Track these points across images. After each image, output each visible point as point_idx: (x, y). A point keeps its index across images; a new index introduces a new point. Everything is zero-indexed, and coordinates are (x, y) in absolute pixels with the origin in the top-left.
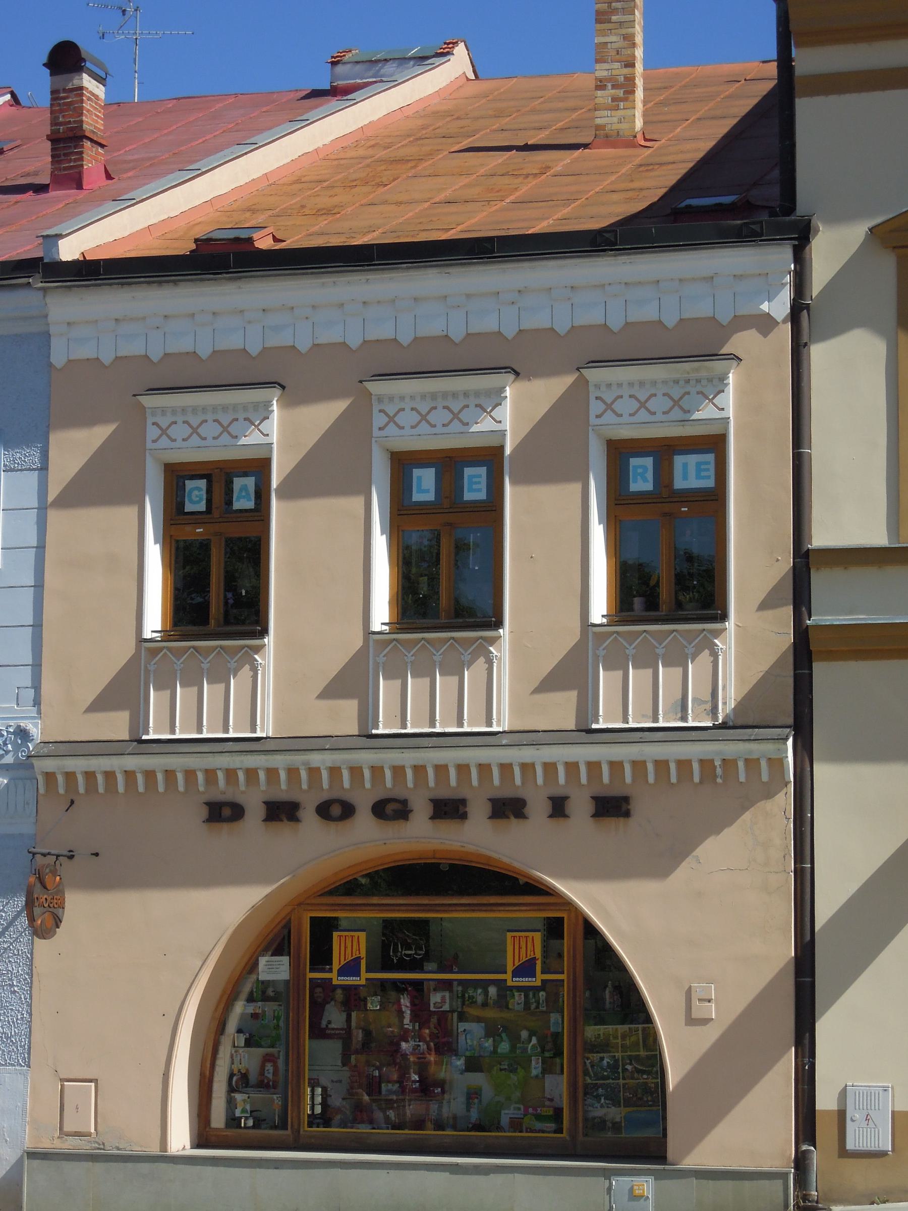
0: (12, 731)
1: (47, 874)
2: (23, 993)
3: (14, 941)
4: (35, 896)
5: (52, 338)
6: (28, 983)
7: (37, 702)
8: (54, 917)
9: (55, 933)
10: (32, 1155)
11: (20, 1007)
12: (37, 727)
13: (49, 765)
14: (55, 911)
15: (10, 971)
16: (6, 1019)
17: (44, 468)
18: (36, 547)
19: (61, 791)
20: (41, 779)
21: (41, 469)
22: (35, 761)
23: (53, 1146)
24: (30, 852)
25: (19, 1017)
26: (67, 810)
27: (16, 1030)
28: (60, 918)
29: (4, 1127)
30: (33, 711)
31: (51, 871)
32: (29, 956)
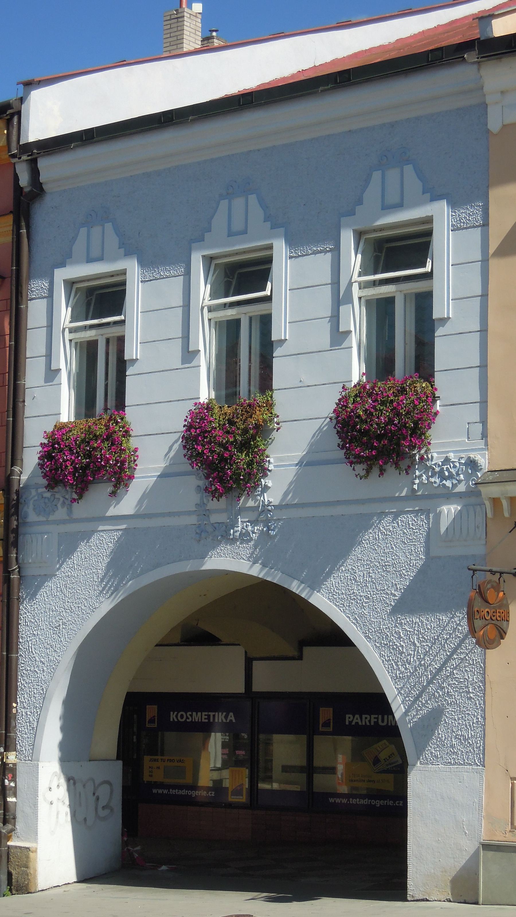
0: (464, 462)
1: (488, 589)
2: (478, 699)
3: (469, 652)
4: (476, 609)
5: (488, 107)
6: (482, 690)
7: (484, 435)
8: (496, 627)
9: (499, 644)
10: (487, 847)
11: (476, 712)
12: (484, 458)
13: (494, 491)
14: (498, 623)
15: (467, 679)
16: (464, 723)
17: (485, 225)
18: (481, 296)
19: (506, 514)
20: (487, 503)
21: (484, 225)
22: (481, 488)
23: (505, 839)
24: (469, 569)
25: (475, 721)
26: (510, 532)
27: (472, 732)
28: (504, 630)
29: (463, 821)
30: (481, 444)
31: (493, 587)
32: (482, 666)
